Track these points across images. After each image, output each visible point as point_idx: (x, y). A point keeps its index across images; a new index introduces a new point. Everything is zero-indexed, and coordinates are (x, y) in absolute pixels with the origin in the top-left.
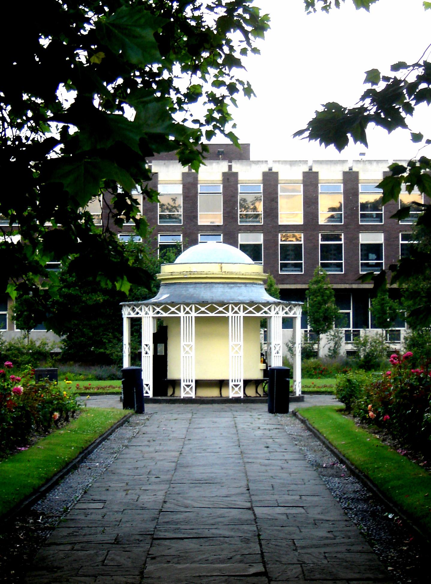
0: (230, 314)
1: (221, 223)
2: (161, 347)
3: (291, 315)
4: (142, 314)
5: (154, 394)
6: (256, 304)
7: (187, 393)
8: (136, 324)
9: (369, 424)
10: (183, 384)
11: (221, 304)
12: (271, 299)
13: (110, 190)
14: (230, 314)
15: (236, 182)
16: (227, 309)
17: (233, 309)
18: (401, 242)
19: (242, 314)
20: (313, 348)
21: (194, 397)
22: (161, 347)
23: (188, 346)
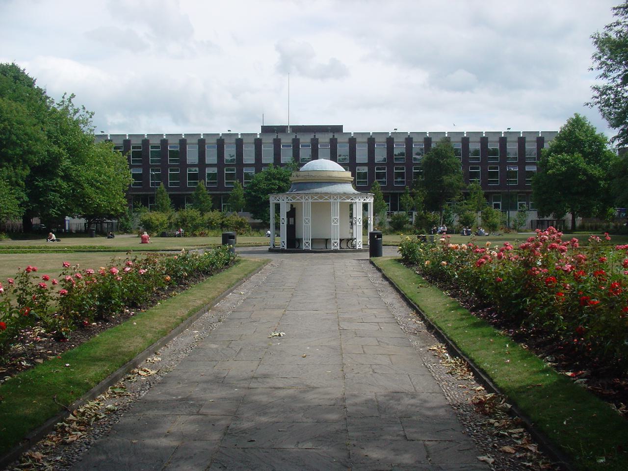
0: (332, 201)
1: (245, 162)
2: (291, 220)
4: (281, 201)
5: (287, 247)
6: (347, 194)
7: (307, 247)
8: (278, 207)
10: (332, 241)
12: (356, 192)
14: (332, 201)
15: (336, 142)
18: (376, 171)
21: (311, 249)
22: (291, 220)
23: (307, 219)
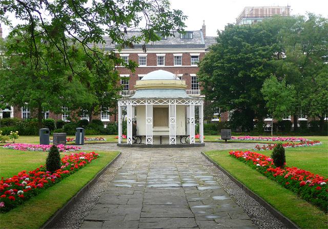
3: (199, 104)
9: (246, 77)
11: (165, 99)
13: (272, 145)
14: (146, 104)
16: (145, 102)
17: (147, 102)
19: (176, 104)
20: (261, 95)
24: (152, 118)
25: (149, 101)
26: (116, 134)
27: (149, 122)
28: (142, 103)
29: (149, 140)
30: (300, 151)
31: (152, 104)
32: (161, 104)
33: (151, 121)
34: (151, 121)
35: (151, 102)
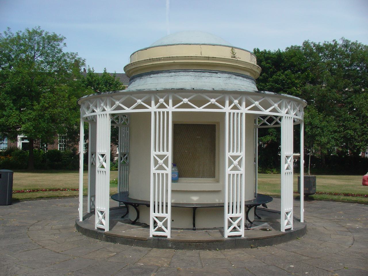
19: (244, 110)
24: (169, 154)
25: (161, 100)
26: (148, 228)
27: (161, 168)
28: (140, 107)
29: (160, 224)
30: (15, 254)
31: (171, 109)
32: (201, 109)
33: (166, 162)
34: (166, 162)
35: (167, 102)
